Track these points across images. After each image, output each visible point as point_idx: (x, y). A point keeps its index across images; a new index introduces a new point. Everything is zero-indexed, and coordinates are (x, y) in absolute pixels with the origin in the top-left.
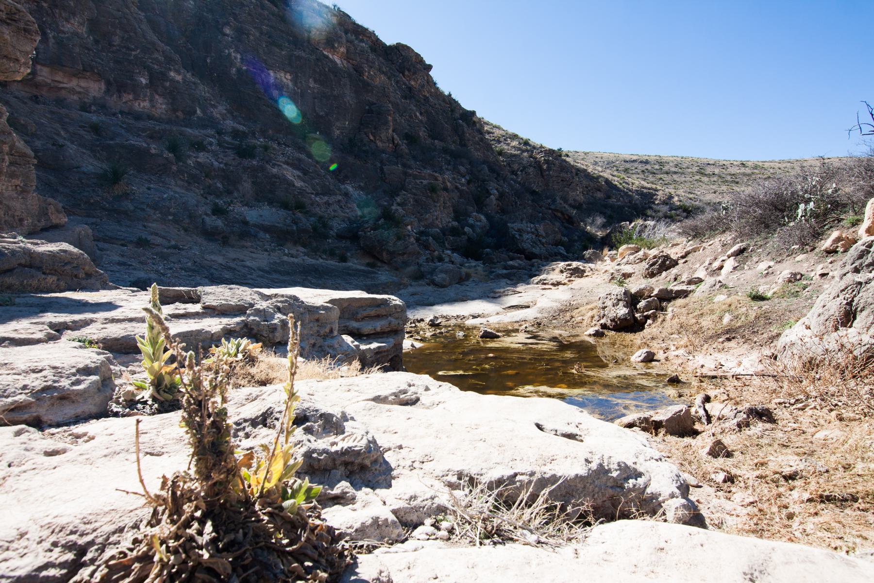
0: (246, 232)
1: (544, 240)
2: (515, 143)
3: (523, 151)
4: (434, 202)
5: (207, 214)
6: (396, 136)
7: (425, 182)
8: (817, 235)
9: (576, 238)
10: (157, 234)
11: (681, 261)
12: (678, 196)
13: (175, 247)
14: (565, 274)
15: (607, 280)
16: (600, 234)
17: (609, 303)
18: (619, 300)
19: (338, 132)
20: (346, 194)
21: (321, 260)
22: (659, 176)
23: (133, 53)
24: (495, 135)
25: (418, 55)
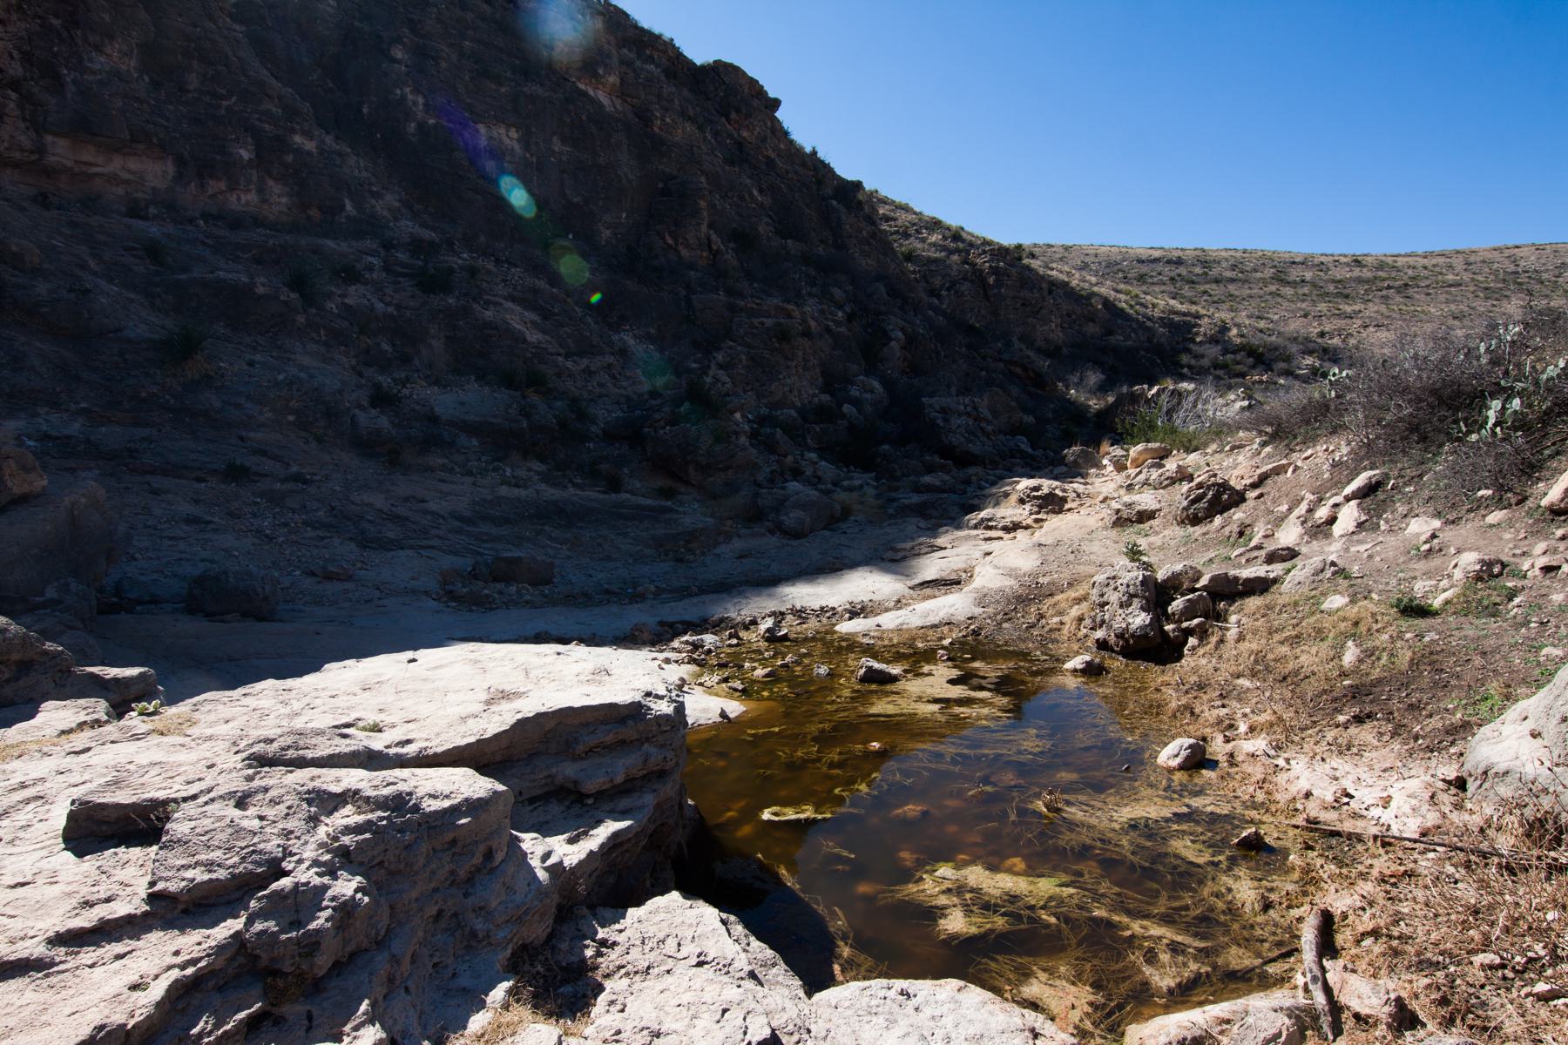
0: (433, 436)
1: (990, 428)
2: (935, 238)
3: (951, 252)
4: (787, 359)
5: (360, 407)
6: (714, 237)
7: (769, 322)
8: (1532, 469)
9: (1050, 415)
10: (264, 453)
11: (1251, 494)
12: (1238, 325)
13: (298, 478)
14: (1028, 507)
15: (1109, 523)
16: (1095, 404)
17: (1114, 597)
18: (1132, 596)
19: (608, 232)
20: (623, 352)
21: (572, 490)
22: (1202, 288)
23: (225, 103)
24: (899, 223)
25: (753, 83)
